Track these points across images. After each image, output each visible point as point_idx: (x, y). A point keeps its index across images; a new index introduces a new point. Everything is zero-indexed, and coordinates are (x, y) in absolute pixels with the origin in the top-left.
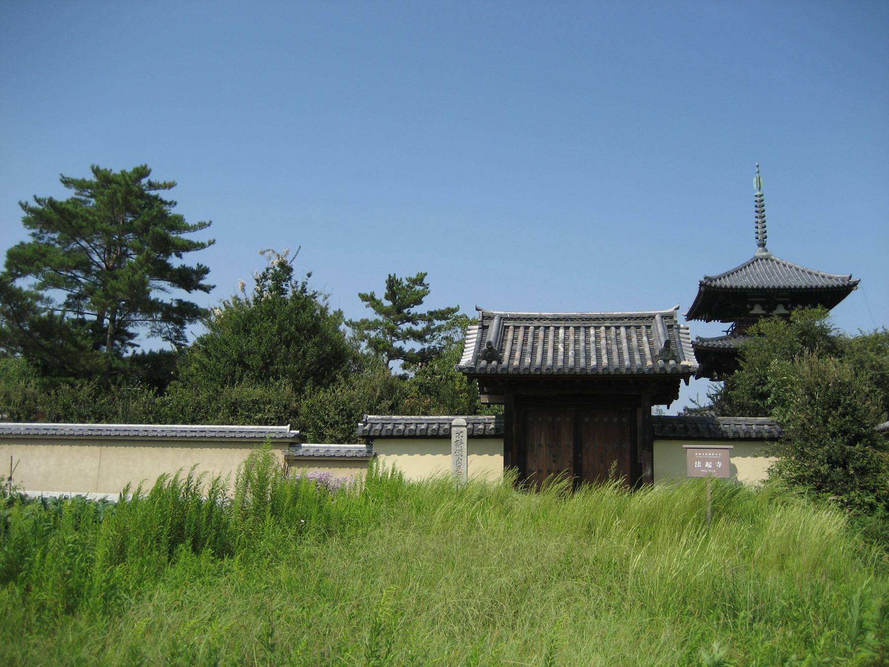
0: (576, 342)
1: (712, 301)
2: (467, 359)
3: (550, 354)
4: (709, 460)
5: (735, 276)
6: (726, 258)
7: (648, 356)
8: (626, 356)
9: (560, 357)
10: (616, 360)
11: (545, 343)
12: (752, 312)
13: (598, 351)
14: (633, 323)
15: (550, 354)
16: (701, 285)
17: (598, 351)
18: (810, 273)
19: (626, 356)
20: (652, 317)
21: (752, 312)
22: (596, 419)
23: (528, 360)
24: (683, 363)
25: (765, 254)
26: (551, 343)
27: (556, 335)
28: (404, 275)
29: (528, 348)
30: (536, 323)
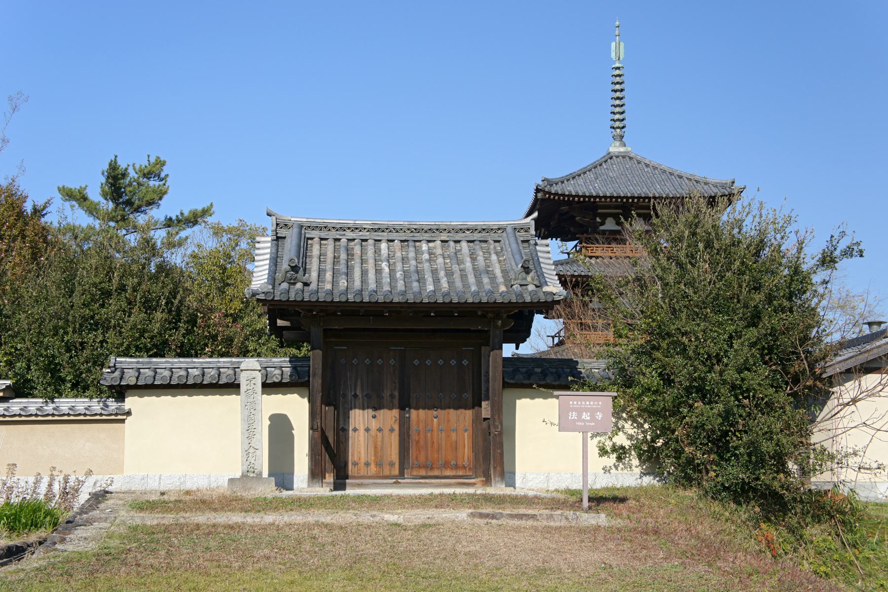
0: (404, 260)
1: (560, 214)
2: (259, 278)
3: (371, 275)
4: (587, 410)
5: (580, 181)
6: (571, 156)
7: (500, 279)
8: (471, 279)
9: (386, 280)
10: (459, 284)
11: (363, 261)
12: (602, 228)
13: (434, 272)
14: (477, 236)
15: (371, 275)
16: (538, 190)
17: (434, 272)
18: (681, 177)
19: (471, 279)
20: (502, 229)
21: (602, 228)
22: (428, 362)
23: (343, 283)
24: (546, 289)
25: (622, 149)
26: (371, 262)
27: (377, 251)
28: (132, 161)
29: (342, 267)
30: (350, 234)
